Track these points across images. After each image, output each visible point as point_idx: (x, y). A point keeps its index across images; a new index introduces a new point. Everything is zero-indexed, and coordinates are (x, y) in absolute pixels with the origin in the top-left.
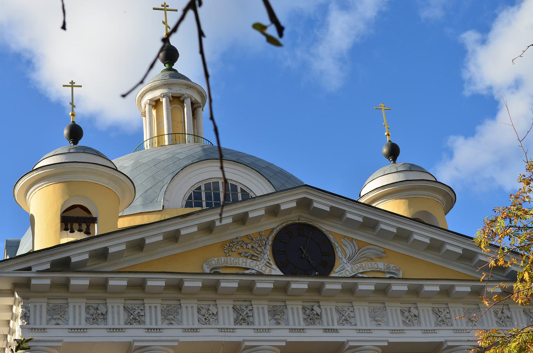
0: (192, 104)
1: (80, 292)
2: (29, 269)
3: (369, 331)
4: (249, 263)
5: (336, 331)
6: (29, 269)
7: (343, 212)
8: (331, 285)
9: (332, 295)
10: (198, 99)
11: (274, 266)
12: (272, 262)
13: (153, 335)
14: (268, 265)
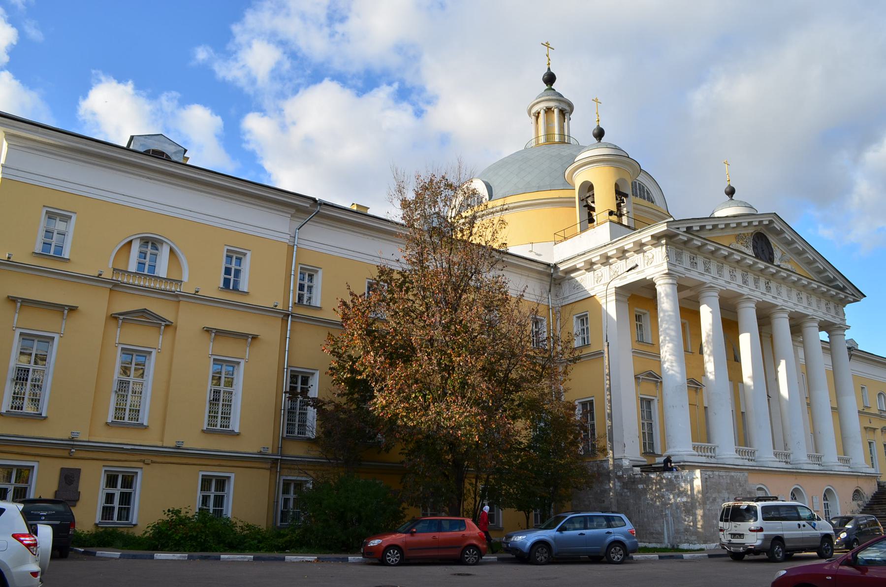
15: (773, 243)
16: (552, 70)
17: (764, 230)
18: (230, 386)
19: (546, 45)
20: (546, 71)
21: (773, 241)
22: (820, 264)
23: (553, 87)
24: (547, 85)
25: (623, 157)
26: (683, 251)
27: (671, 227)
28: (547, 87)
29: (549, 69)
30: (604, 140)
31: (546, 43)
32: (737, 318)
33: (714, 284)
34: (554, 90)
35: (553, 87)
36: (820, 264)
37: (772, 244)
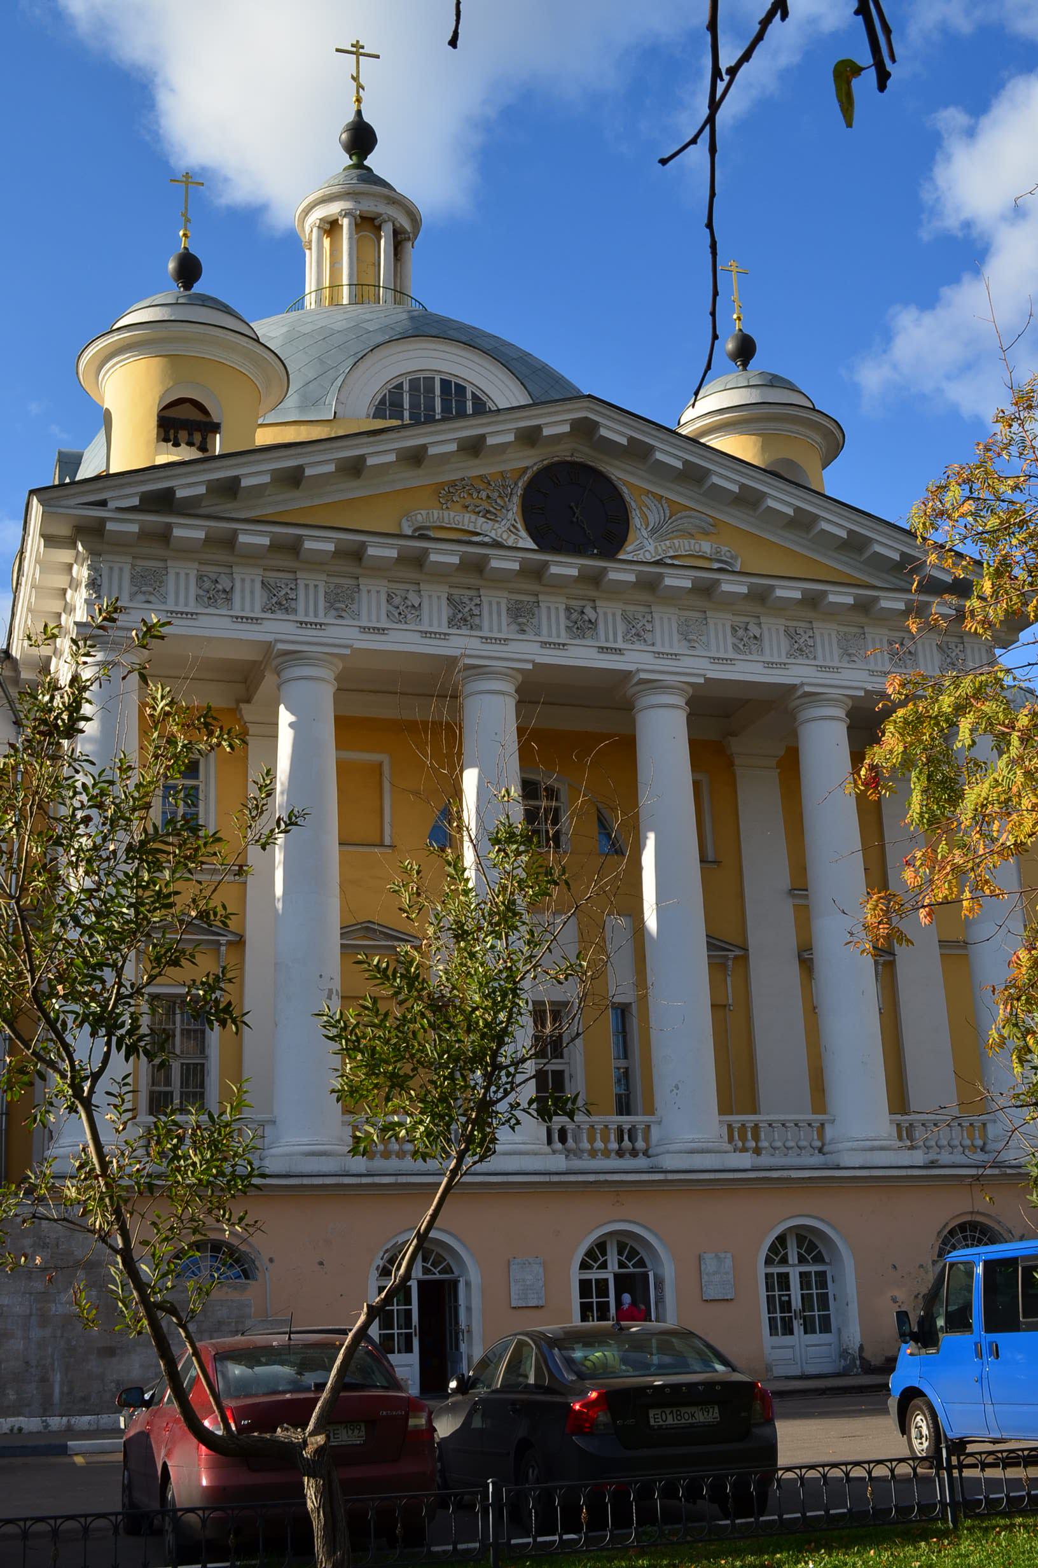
0: (396, 233)
2: (103, 503)
4: (480, 524)
6: (103, 503)
8: (618, 574)
10: (407, 225)
11: (523, 533)
13: (310, 634)
14: (513, 529)
15: (625, 483)
16: (367, 118)
17: (587, 450)
18: (806, 1297)
19: (354, 49)
20: (351, 117)
21: (621, 475)
22: (829, 521)
23: (366, 163)
24: (351, 158)
25: (211, 328)
26: (169, 563)
27: (65, 503)
28: (351, 163)
30: (198, 288)
31: (353, 46)
32: (797, 742)
33: (293, 642)
34: (368, 169)
35: (366, 163)
36: (829, 521)
37: (625, 490)
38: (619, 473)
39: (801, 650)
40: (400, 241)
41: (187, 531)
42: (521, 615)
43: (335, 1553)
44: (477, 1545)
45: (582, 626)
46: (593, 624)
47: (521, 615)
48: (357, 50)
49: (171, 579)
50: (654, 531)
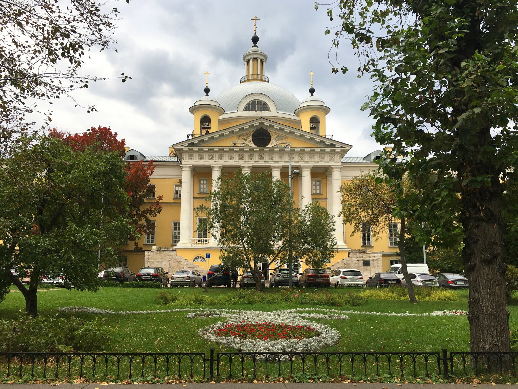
0: (261, 60)
1: (196, 151)
2: (183, 146)
3: (278, 162)
4: (244, 142)
5: (268, 162)
6: (183, 146)
7: (273, 126)
8: (266, 149)
9: (267, 152)
10: (263, 58)
11: (252, 143)
12: (251, 141)
13: (216, 163)
14: (250, 142)
16: (258, 35)
20: (253, 35)
29: (255, 33)
38: (269, 130)
39: (302, 159)
40: (262, 62)
41: (196, 149)
42: (251, 157)
43: (217, 272)
44: (450, 152)
45: (262, 158)
46: (263, 158)
47: (251, 157)
48: (255, 19)
49: (194, 156)
50: (275, 140)
